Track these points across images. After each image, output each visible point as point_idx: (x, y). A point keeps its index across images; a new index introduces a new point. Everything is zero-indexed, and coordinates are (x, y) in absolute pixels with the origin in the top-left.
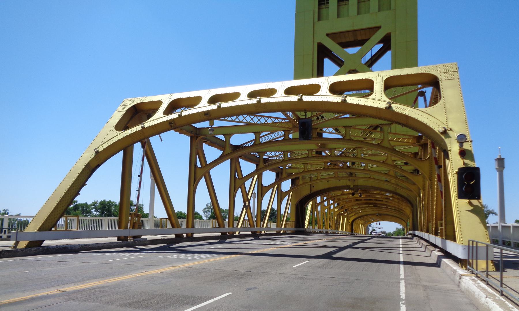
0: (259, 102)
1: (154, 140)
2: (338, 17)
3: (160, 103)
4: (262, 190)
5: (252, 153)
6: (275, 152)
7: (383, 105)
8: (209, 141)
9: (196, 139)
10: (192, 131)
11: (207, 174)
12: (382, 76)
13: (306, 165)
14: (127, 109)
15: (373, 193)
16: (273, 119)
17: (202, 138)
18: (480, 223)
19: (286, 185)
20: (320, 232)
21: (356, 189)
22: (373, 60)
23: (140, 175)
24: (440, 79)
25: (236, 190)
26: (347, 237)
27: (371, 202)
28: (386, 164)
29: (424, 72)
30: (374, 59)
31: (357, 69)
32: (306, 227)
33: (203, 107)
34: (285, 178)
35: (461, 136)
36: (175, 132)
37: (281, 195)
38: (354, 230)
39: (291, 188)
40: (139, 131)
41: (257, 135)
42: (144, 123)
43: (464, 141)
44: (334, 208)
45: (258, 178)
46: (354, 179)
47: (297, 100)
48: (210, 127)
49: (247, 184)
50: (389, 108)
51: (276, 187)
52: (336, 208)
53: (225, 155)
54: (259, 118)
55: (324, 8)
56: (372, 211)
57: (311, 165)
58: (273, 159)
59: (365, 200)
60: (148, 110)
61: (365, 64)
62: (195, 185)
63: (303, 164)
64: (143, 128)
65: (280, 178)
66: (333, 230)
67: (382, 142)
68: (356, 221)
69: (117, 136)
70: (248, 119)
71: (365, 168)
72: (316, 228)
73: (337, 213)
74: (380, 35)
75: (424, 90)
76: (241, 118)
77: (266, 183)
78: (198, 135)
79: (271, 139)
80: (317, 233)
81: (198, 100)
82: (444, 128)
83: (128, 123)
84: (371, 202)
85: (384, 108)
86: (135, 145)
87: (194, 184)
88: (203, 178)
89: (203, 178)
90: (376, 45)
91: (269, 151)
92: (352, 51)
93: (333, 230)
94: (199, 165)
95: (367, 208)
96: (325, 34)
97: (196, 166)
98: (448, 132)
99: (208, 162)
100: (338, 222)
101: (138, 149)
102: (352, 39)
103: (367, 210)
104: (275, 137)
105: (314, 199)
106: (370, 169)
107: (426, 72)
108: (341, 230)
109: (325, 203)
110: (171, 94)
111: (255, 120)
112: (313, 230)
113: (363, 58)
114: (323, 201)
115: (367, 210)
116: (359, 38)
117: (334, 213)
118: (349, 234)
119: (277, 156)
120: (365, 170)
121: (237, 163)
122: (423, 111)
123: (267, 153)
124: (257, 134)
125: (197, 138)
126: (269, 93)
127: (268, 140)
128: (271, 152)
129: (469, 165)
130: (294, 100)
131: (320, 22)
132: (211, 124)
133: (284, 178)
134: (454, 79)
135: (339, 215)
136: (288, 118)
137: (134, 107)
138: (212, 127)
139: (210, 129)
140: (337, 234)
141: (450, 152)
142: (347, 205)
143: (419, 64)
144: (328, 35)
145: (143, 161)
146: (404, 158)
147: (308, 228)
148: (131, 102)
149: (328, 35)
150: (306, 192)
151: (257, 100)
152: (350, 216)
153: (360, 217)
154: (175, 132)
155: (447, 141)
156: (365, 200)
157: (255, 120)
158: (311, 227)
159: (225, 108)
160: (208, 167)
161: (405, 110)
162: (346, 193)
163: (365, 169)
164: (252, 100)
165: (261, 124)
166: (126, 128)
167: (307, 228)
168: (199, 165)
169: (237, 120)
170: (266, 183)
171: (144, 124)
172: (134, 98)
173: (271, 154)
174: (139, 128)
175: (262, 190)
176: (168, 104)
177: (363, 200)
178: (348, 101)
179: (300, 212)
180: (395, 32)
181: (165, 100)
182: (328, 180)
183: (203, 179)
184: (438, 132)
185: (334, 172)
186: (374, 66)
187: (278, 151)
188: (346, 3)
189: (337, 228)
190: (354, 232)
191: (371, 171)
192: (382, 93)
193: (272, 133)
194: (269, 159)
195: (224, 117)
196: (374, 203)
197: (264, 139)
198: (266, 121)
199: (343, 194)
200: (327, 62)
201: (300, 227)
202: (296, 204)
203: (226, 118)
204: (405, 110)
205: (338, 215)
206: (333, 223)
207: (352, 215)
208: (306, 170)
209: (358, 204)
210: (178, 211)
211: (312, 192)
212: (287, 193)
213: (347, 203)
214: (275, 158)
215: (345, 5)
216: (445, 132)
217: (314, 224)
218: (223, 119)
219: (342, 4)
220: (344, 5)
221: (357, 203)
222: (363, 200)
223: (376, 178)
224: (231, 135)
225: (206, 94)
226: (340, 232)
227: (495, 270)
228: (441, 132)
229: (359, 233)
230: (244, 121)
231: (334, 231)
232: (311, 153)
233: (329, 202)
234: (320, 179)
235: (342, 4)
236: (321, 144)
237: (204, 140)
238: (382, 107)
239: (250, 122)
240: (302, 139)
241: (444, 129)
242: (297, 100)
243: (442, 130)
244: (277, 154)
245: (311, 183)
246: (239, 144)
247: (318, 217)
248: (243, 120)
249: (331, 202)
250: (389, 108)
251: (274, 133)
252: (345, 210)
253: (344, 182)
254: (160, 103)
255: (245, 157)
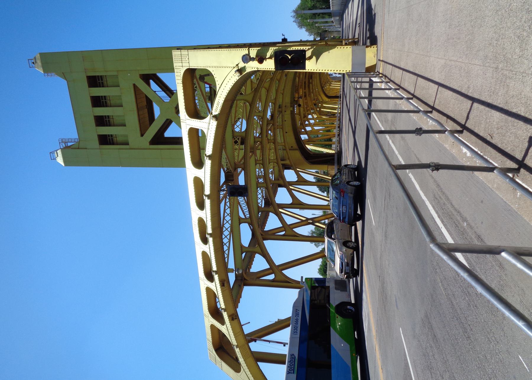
0: (211, 235)
1: (247, 330)
2: (125, 125)
3: (212, 327)
4: (297, 204)
5: (259, 216)
6: (258, 194)
7: (214, 123)
8: (248, 266)
9: (247, 280)
10: (239, 285)
11: (280, 268)
12: (185, 120)
13: (271, 161)
14: (219, 359)
15: (298, 83)
16: (227, 207)
17: (245, 273)
18: (329, 52)
19: (290, 175)
20: (339, 135)
21: (294, 102)
22: (167, 90)
23: (283, 345)
24: (189, 68)
25: (303, 204)
26: (343, 115)
27: (307, 83)
28: (269, 88)
29: (182, 81)
30: (165, 89)
31: (175, 106)
32: (333, 152)
33: (216, 286)
34: (283, 182)
35: (244, 57)
36: (239, 303)
37: (302, 181)
38: (336, 94)
39: (292, 170)
40: (240, 351)
41: (242, 221)
42: (233, 345)
43: (248, 57)
44: (313, 119)
45: (282, 208)
46: (284, 107)
47: (209, 200)
48: (234, 272)
49: (290, 221)
50: (215, 117)
51: (291, 187)
52: (313, 116)
53: (262, 252)
54: (225, 222)
55: (116, 139)
56: (316, 78)
57: (271, 150)
58: (264, 194)
59: (305, 89)
60: (219, 335)
61: (170, 97)
62: (292, 283)
63: (269, 163)
64: (237, 347)
65: (282, 183)
66: (336, 120)
67: (247, 101)
68: (326, 92)
69: (246, 372)
70: (226, 233)
71: (273, 103)
72: (334, 140)
73: (319, 116)
74: (142, 85)
75: (198, 77)
76: (225, 241)
77: (288, 200)
78: (242, 278)
79: (245, 204)
80: (340, 139)
81: (208, 290)
82: (236, 72)
83: (233, 358)
84: (307, 83)
85: (217, 122)
86: (252, 350)
87: (291, 283)
88: (284, 272)
89: (284, 272)
90: (152, 88)
91: (257, 200)
92: (157, 111)
93: (336, 120)
94: (271, 277)
95: (313, 84)
96: (142, 137)
97: (273, 281)
98: (239, 68)
99: (268, 267)
100: (327, 114)
101: (256, 346)
102: (146, 110)
103: (316, 84)
104: (244, 201)
105: (303, 143)
106: (274, 98)
107: (182, 79)
108: (335, 110)
109: (307, 130)
110: (200, 278)
111: (227, 226)
112: (337, 143)
113: (165, 101)
114: (306, 133)
115: (316, 84)
116: (145, 103)
117: (318, 119)
118: (341, 101)
119: (262, 192)
120: (275, 102)
121: (270, 233)
122: (220, 88)
123: (259, 202)
124: (241, 221)
125: (245, 279)
126: (202, 223)
127: (246, 207)
128: (258, 198)
129: (271, 54)
130: (209, 202)
131: (130, 143)
132: (232, 271)
133: (284, 183)
134: (188, 55)
135: (321, 113)
136: (225, 197)
137: (217, 350)
138: (234, 270)
139: (237, 273)
140: (340, 115)
141: (259, 68)
142: (311, 106)
143: (177, 136)
144: (142, 135)
145: (269, 341)
146: (263, 80)
147: (334, 149)
148: (212, 354)
149: (142, 135)
150: (297, 155)
151: (207, 199)
152: (321, 100)
153: (322, 88)
154: (239, 303)
155: (248, 70)
156: (305, 89)
157: (227, 226)
158: (334, 146)
159: (217, 267)
160: (273, 268)
161: (218, 103)
162: (298, 110)
163: (274, 102)
164: (209, 242)
165: (232, 220)
166: (237, 359)
167: (334, 150)
168: (271, 277)
169: (228, 244)
170: (288, 200)
171: (234, 345)
172: (208, 350)
173: (259, 198)
174: (237, 350)
175: (297, 204)
176: (209, 282)
177: (305, 91)
178: (210, 154)
179: (316, 160)
180: (138, 70)
181: (210, 322)
182: (284, 121)
183: (285, 272)
184: (239, 77)
185: (277, 129)
186: (172, 88)
187: (257, 191)
188: (112, 118)
189: (334, 115)
190: (338, 95)
191: (276, 96)
192: (201, 122)
193: (239, 203)
194: (265, 197)
195: (224, 252)
196: (308, 79)
197: (244, 208)
198: (228, 215)
199: (299, 114)
200: (168, 134)
201: (334, 159)
202: (311, 165)
203: (226, 256)
204: (218, 103)
205: (320, 114)
206: (330, 120)
207: (320, 98)
208: (275, 161)
209: (310, 94)
210: (318, 272)
211: (297, 148)
212: (299, 176)
213: (308, 106)
214: (264, 192)
215: (113, 118)
216: (240, 71)
217: (330, 143)
218: (226, 259)
219: (112, 121)
220: (113, 120)
221: (308, 95)
222: (305, 91)
223: (283, 88)
224: (242, 246)
225: (204, 283)
226: (338, 111)
227: (376, 46)
228: (239, 74)
229: (339, 89)
230: (228, 237)
231: (337, 119)
232: (258, 161)
233: (307, 125)
234: (285, 143)
235: (112, 121)
236: (251, 152)
237: (248, 271)
238: (216, 124)
239: (230, 224)
240: (246, 194)
241: (237, 72)
242: (209, 200)
243: (238, 74)
244: (260, 191)
245: (288, 150)
246: (251, 232)
247: (323, 129)
248: (228, 231)
249: (307, 123)
250: (215, 117)
251: (240, 201)
252: (316, 106)
253: (287, 116)
254: (212, 327)
255: (263, 224)
